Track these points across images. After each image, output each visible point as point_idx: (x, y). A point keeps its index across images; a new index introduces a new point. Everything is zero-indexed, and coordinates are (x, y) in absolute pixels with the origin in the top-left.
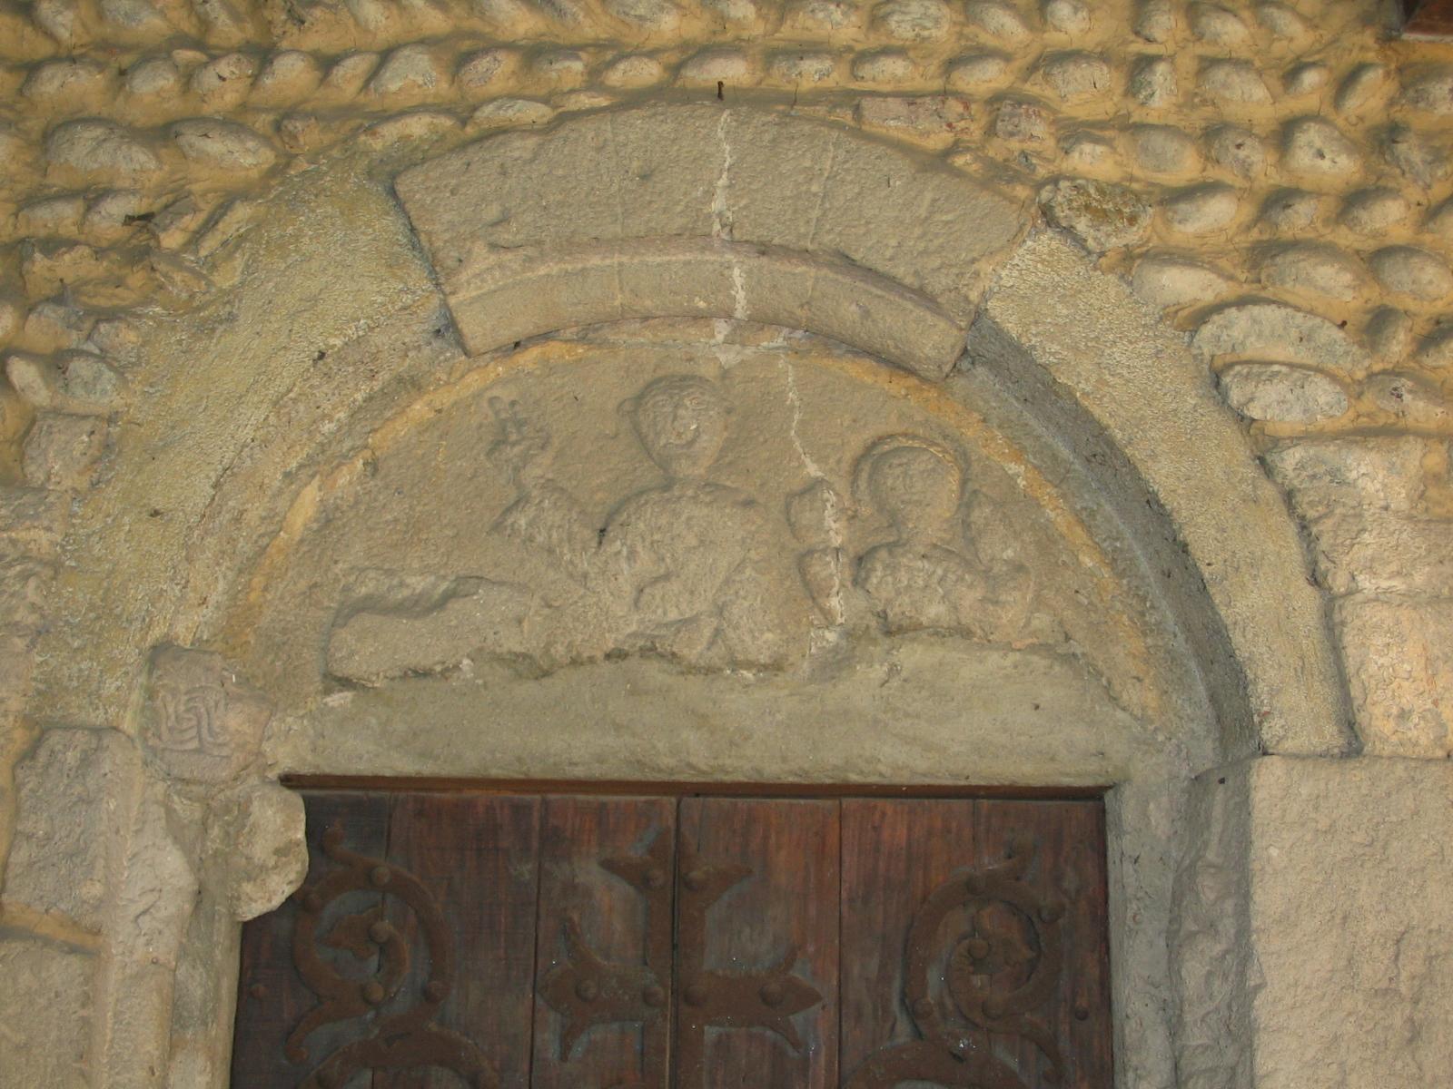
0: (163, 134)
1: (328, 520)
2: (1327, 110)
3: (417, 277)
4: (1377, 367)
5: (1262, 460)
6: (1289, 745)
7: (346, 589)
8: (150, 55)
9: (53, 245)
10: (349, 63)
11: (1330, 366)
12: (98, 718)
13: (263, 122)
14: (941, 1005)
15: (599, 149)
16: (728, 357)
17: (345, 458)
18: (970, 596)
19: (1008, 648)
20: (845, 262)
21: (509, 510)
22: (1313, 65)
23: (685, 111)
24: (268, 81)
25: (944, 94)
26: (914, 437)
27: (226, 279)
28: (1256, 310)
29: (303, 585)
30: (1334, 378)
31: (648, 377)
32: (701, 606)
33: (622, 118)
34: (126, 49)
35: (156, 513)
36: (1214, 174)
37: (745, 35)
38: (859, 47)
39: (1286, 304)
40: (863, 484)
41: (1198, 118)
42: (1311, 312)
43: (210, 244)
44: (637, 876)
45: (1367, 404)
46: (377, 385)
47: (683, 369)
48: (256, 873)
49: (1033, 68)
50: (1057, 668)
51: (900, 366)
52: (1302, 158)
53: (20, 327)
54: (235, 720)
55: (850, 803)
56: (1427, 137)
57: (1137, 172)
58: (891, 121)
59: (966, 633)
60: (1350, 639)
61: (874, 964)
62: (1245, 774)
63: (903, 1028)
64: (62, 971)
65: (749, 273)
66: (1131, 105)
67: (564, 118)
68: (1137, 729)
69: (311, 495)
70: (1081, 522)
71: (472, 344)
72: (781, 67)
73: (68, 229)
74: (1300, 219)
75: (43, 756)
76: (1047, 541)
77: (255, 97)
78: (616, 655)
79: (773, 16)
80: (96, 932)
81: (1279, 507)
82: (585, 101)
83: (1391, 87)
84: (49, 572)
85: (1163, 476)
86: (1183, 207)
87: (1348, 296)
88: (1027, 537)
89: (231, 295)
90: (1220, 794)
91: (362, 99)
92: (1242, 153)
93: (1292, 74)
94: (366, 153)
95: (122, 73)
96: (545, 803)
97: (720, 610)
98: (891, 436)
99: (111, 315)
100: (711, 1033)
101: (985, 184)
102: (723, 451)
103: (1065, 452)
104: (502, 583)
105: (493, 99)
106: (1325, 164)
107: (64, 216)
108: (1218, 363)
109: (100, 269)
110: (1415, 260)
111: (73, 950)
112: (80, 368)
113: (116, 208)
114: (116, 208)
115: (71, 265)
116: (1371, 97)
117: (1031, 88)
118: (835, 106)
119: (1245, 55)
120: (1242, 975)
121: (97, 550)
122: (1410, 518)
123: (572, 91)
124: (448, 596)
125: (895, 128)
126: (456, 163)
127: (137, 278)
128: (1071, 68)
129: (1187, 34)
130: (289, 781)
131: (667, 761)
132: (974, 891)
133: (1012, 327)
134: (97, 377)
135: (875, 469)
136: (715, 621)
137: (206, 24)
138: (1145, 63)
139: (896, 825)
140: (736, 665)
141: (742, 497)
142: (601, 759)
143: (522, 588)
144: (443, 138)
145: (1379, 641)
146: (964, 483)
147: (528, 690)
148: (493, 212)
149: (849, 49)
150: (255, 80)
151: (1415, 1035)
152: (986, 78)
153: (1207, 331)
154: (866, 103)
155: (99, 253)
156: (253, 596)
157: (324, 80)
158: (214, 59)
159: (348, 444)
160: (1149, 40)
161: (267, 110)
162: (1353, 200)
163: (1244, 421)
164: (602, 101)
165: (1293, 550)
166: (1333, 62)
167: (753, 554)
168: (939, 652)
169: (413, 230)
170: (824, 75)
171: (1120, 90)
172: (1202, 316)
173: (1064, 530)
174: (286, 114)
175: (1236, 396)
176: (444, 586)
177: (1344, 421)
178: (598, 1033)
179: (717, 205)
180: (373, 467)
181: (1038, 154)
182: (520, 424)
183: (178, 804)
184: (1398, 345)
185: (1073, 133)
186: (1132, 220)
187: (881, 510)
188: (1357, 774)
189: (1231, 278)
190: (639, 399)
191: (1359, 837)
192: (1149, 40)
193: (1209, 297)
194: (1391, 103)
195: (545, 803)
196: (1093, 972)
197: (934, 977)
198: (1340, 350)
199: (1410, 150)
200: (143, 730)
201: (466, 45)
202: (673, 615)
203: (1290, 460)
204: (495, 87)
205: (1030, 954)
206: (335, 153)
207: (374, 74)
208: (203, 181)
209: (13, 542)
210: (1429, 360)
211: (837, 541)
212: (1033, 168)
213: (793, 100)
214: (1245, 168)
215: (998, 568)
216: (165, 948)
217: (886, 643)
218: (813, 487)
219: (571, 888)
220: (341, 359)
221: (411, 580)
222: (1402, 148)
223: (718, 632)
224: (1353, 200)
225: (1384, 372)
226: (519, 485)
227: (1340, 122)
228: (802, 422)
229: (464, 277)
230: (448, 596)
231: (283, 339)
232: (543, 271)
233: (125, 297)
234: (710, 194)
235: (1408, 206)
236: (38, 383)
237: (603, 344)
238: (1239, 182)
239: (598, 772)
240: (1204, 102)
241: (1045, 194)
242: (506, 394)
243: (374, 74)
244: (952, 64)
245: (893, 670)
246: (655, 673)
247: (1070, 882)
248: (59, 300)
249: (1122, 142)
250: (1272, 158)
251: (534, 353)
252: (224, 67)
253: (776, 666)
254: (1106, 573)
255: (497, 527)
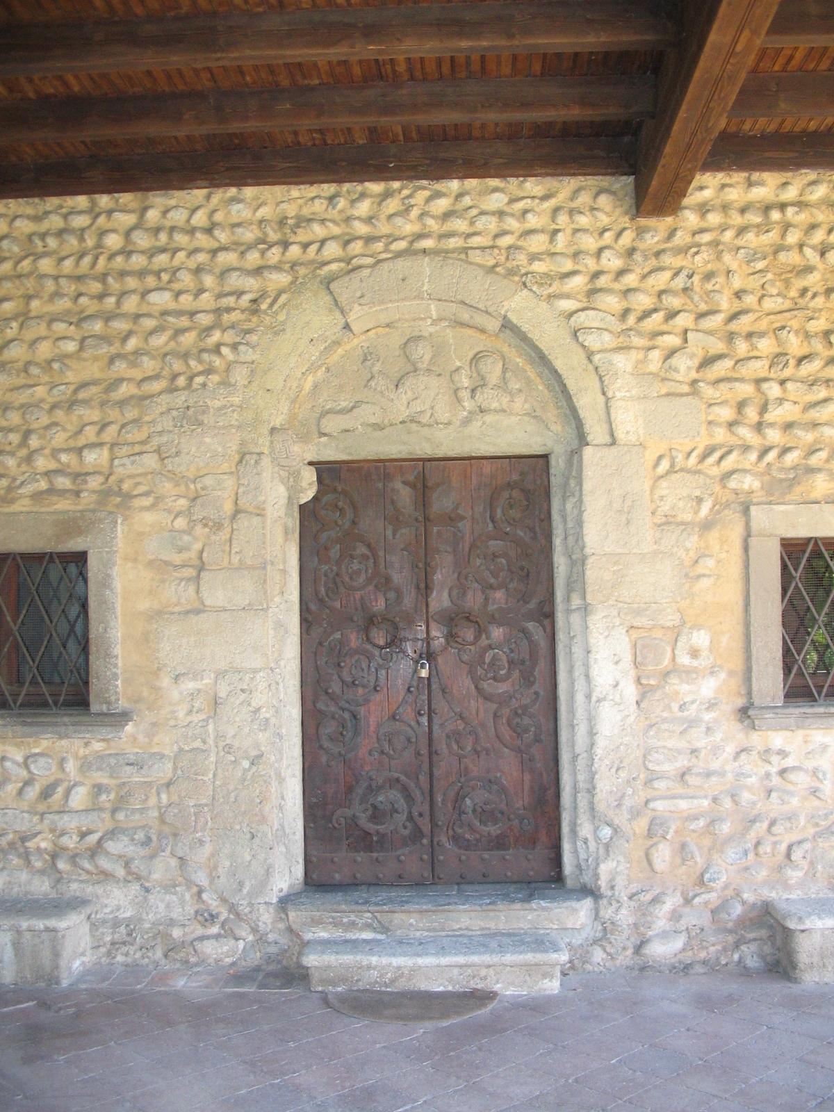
0: (258, 271)
1: (316, 386)
2: (613, 244)
3: (338, 314)
4: (624, 328)
5: (589, 358)
6: (595, 442)
7: (323, 407)
8: (250, 247)
9: (229, 310)
10: (311, 247)
11: (610, 328)
12: (258, 450)
13: (287, 267)
14: (502, 520)
15: (390, 271)
16: (432, 329)
17: (320, 367)
18: (505, 400)
19: (518, 414)
20: (463, 303)
21: (369, 381)
22: (608, 230)
23: (415, 257)
24: (287, 254)
25: (493, 247)
26: (488, 352)
27: (281, 317)
28: (587, 312)
29: (310, 406)
30: (610, 332)
31: (408, 337)
32: (427, 406)
33: (395, 261)
34: (242, 244)
35: (268, 390)
36: (577, 268)
37: (432, 230)
38: (467, 232)
39: (597, 309)
40: (473, 368)
41: (572, 250)
42: (605, 312)
43: (275, 307)
44: (413, 486)
45: (621, 339)
46: (327, 344)
47: (420, 334)
48: (303, 491)
49: (521, 236)
50: (532, 420)
51: (483, 331)
52: (604, 261)
53: (222, 336)
54: (296, 448)
55: (473, 461)
56: (643, 251)
57: (553, 268)
58: (476, 257)
59: (504, 411)
60: (612, 411)
61: (482, 508)
62: (581, 451)
63: (491, 525)
64: (256, 520)
65: (436, 306)
66: (551, 246)
67: (379, 261)
68: (555, 438)
69: (310, 380)
70: (539, 376)
71: (355, 332)
72: (443, 241)
73: (232, 305)
74: (603, 281)
75: (244, 462)
76: (529, 382)
77: (284, 259)
78: (403, 422)
79: (440, 223)
80: (264, 509)
81: (594, 372)
82: (384, 256)
83: (634, 235)
84: (239, 409)
85: (559, 364)
86: (566, 280)
87: (617, 305)
88: (523, 381)
89: (283, 323)
90: (576, 456)
91: (317, 258)
92: (585, 261)
93: (602, 233)
94: (319, 275)
95: (242, 253)
96: (384, 465)
97: (432, 408)
98: (482, 352)
99: (248, 332)
100: (435, 529)
101: (505, 277)
102: (432, 359)
103: (533, 355)
104: (368, 403)
105: (356, 257)
106: (611, 263)
107: (230, 301)
108: (576, 329)
109: (243, 317)
110: (637, 294)
111: (258, 515)
112: (241, 348)
113: (247, 298)
114: (247, 298)
115: (235, 316)
116: (627, 239)
117: (520, 243)
118: (461, 253)
119: (587, 227)
120: (580, 508)
121: (253, 402)
122: (632, 374)
123: (380, 253)
124: (353, 408)
125: (478, 260)
126: (347, 278)
127: (255, 319)
128: (532, 236)
129: (569, 221)
130: (311, 464)
131: (419, 452)
132: (510, 486)
133: (515, 321)
134: (247, 352)
135: (477, 361)
136: (431, 411)
137: (265, 234)
138: (556, 231)
139: (487, 468)
140: (437, 424)
141: (437, 373)
142: (400, 453)
143: (374, 404)
144: (342, 270)
145: (620, 412)
146: (504, 365)
147: (378, 434)
148: (358, 294)
149: (464, 233)
150: (283, 253)
151: (628, 522)
152: (506, 241)
153: (573, 319)
154: (470, 252)
155: (243, 311)
156: (296, 411)
157: (304, 252)
158: (270, 247)
159: (319, 363)
160: (557, 224)
161: (288, 263)
162: (621, 273)
163: (584, 347)
164: (389, 256)
165: (598, 385)
166: (615, 228)
167: (441, 391)
168: (497, 417)
169: (336, 300)
170: (456, 243)
171: (547, 242)
172: (571, 314)
173: (533, 378)
174: (294, 265)
175: (581, 339)
176: (351, 404)
177: (614, 345)
178: (404, 531)
179: (425, 288)
180: (328, 370)
181: (521, 266)
182: (371, 353)
183: (281, 472)
184: (631, 320)
185: (533, 258)
186: (550, 285)
187: (479, 374)
188: (614, 450)
189: (581, 301)
190: (406, 344)
191: (615, 468)
192: (557, 224)
193: (574, 308)
194: (634, 240)
195: (384, 465)
196: (545, 507)
197: (499, 511)
198: (613, 323)
199: (638, 257)
200: (270, 453)
201: (347, 238)
202: (419, 410)
203: (596, 358)
204: (357, 252)
205: (526, 503)
206: (310, 276)
207: (319, 250)
208: (272, 288)
209: (228, 401)
210: (641, 324)
211: (466, 385)
212: (520, 270)
213: (447, 252)
214: (586, 266)
215: (514, 391)
216: (282, 513)
217: (481, 414)
218: (458, 369)
219: (393, 490)
220: (318, 340)
221: (342, 403)
222: (635, 256)
223: (432, 414)
224: (621, 273)
225: (627, 329)
226: (371, 373)
227: (617, 248)
228: (455, 349)
229: (351, 314)
230: (353, 408)
231: (300, 336)
232: (375, 309)
233: (252, 325)
234: (423, 284)
235: (637, 275)
236: (230, 354)
237: (394, 327)
238: (585, 270)
239: (399, 456)
240: (574, 244)
241: (524, 279)
242: (366, 345)
243: (319, 250)
244: (496, 236)
245: (484, 423)
246: (414, 426)
247: (538, 482)
248: (233, 327)
249: (548, 259)
250: (595, 261)
251: (373, 331)
252: (274, 250)
253: (449, 423)
254: (546, 391)
255: (366, 386)
